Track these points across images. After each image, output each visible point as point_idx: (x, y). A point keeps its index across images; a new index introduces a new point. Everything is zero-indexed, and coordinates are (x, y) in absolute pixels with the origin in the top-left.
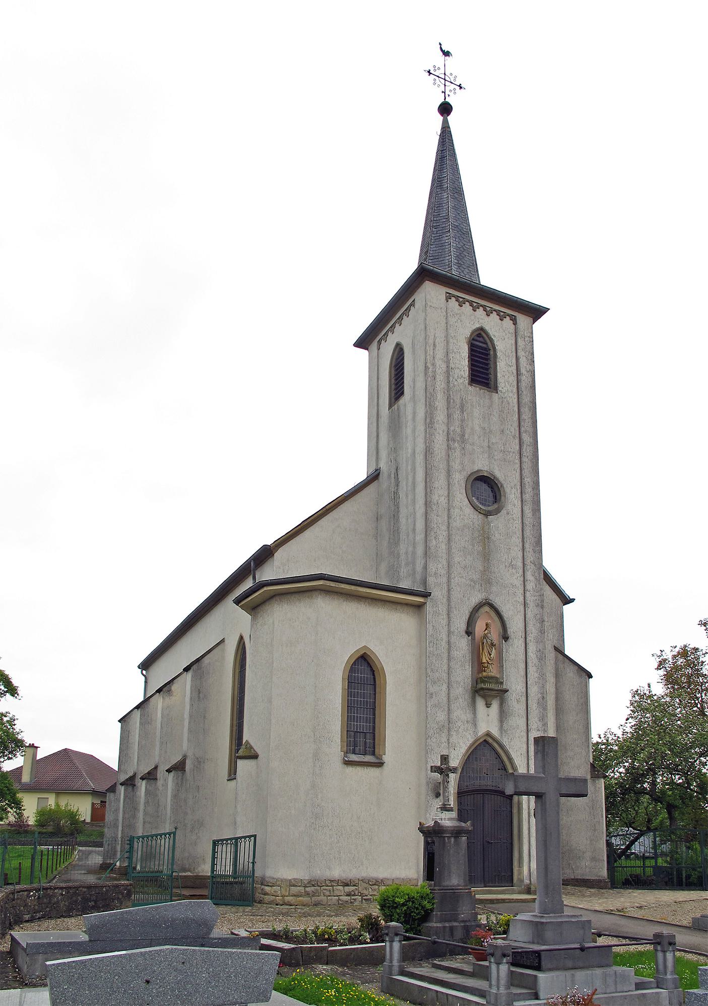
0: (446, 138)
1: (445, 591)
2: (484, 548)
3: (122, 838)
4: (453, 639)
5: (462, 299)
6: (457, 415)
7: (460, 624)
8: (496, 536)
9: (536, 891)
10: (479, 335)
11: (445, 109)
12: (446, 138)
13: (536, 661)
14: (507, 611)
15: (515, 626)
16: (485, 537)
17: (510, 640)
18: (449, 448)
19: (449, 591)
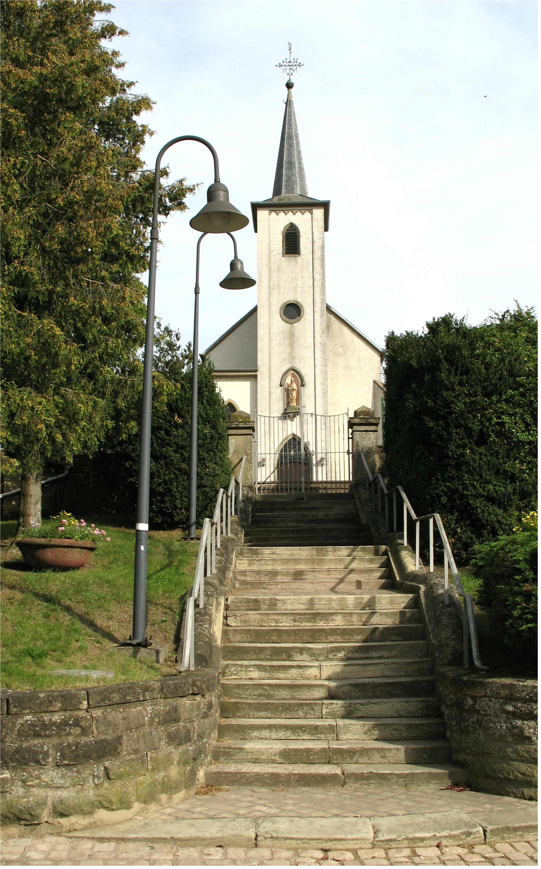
0: (288, 103)
1: (267, 367)
2: (291, 341)
3: (266, 516)
4: (272, 390)
5: (146, 283)
6: (275, 275)
7: (276, 381)
8: (298, 333)
9: (358, 513)
10: (290, 227)
11: (289, 86)
12: (288, 103)
13: (321, 394)
14: (303, 372)
15: (308, 379)
16: (291, 335)
17: (306, 386)
18: (270, 293)
19: (270, 366)
